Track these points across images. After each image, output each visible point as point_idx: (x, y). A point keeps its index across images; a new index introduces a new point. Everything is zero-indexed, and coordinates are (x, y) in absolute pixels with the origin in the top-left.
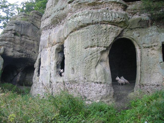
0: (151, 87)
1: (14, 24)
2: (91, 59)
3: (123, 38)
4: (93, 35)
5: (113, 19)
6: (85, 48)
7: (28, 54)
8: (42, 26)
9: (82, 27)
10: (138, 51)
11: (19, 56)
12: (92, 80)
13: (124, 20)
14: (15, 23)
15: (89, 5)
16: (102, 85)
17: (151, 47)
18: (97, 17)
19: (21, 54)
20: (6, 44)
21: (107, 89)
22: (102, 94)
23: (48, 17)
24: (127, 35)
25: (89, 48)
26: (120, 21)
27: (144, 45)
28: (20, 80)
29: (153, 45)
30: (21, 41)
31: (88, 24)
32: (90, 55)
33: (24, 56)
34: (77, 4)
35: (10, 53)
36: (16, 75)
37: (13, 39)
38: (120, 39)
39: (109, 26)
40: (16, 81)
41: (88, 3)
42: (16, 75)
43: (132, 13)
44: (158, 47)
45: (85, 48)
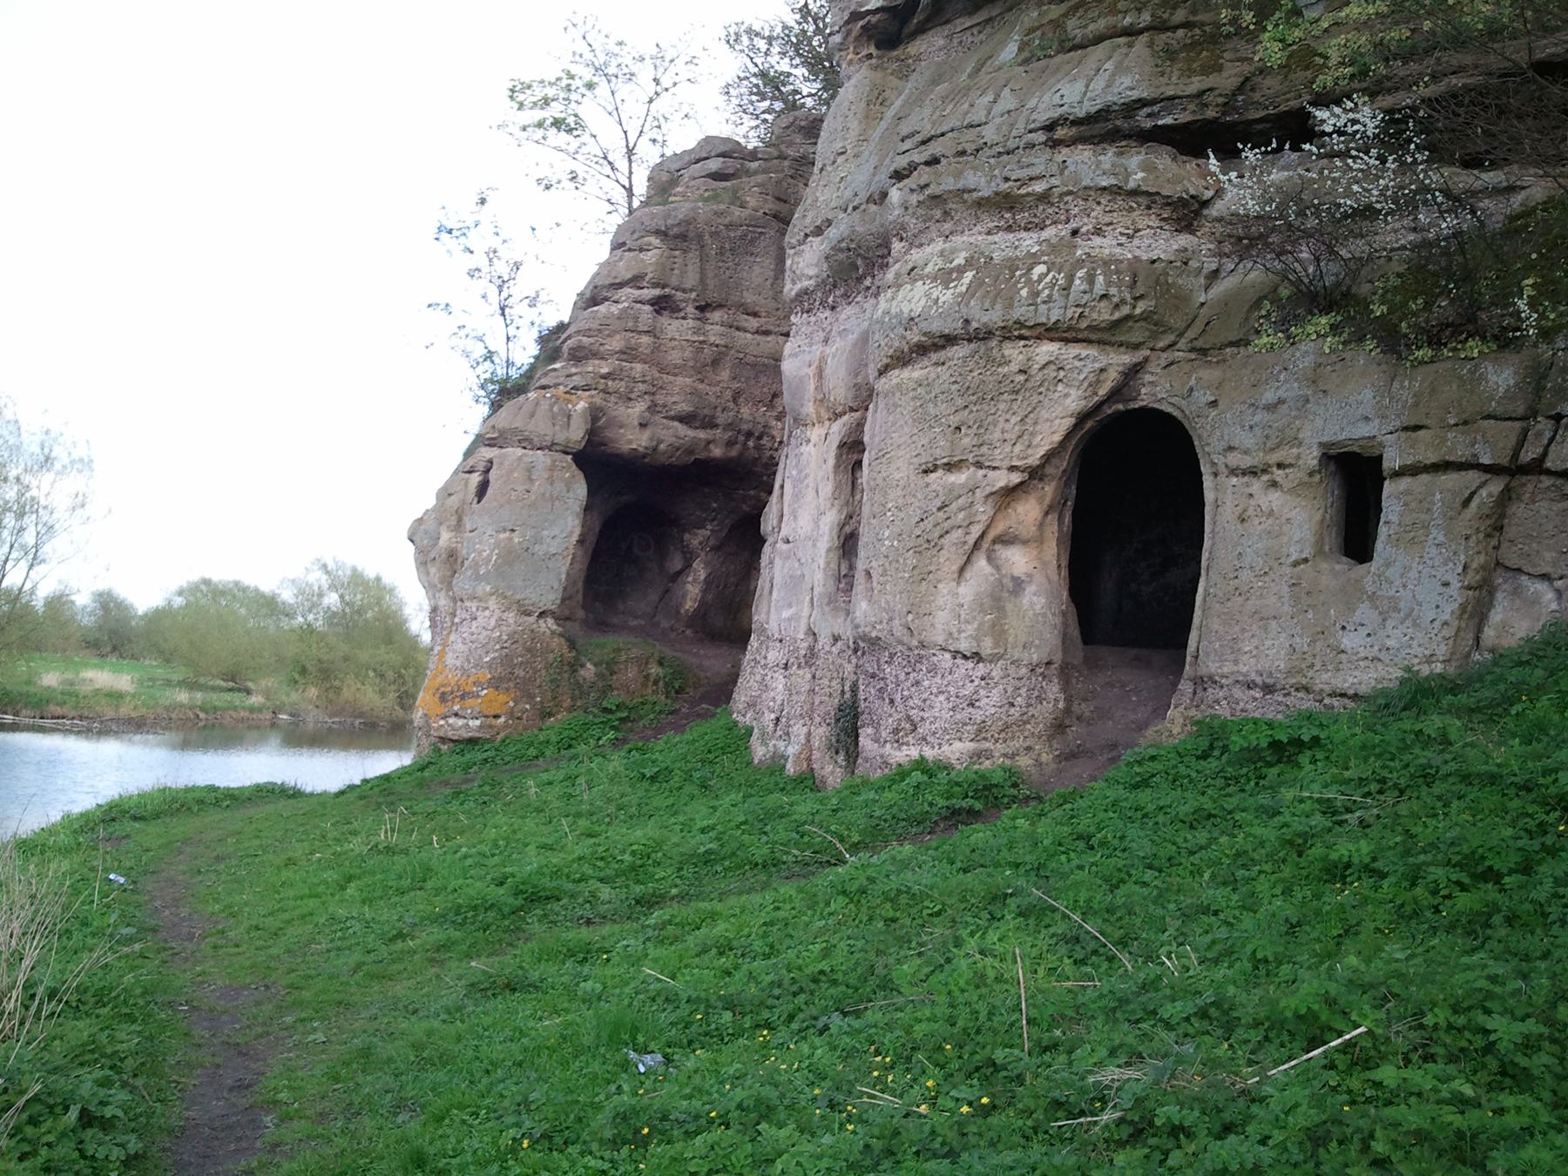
0: (1238, 692)
1: (655, 241)
2: (937, 534)
3: (1143, 409)
4: (960, 402)
5: (1069, 314)
6: (925, 472)
7: (749, 434)
8: (788, 286)
9: (922, 350)
10: (1208, 482)
11: (690, 451)
12: (940, 640)
13: (1138, 311)
14: (657, 232)
15: (980, 204)
16: (982, 669)
17: (1264, 471)
18: (987, 305)
19: (702, 435)
20: (604, 377)
21: (1010, 689)
22: (978, 715)
23: (819, 231)
24: (1155, 391)
25: (940, 472)
26: (1117, 315)
27: (1234, 459)
28: (702, 603)
29: (1274, 458)
30: (700, 350)
31: (950, 340)
32: (939, 509)
33: (717, 452)
34: (921, 198)
35: (632, 439)
36: (680, 573)
37: (645, 339)
38: (1119, 416)
39: (1047, 350)
40: (678, 612)
41: (975, 195)
42: (680, 573)
43: (1240, 239)
44: (1296, 475)
45: (925, 472)
